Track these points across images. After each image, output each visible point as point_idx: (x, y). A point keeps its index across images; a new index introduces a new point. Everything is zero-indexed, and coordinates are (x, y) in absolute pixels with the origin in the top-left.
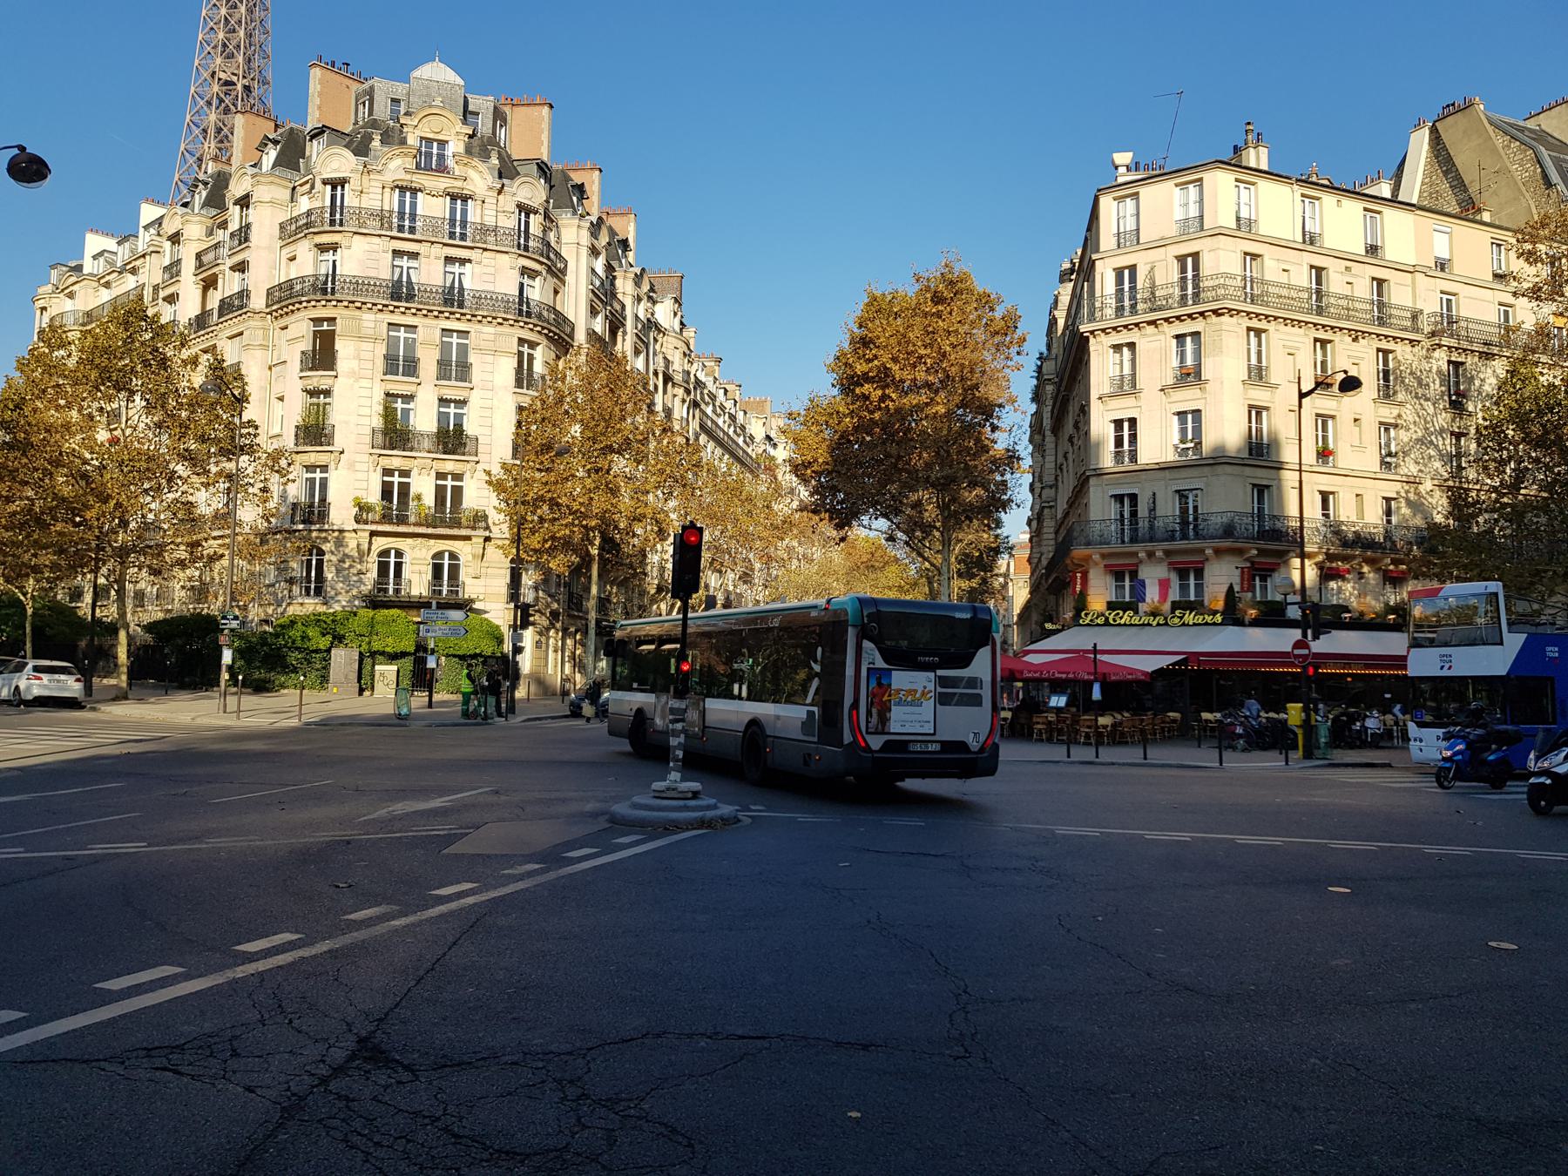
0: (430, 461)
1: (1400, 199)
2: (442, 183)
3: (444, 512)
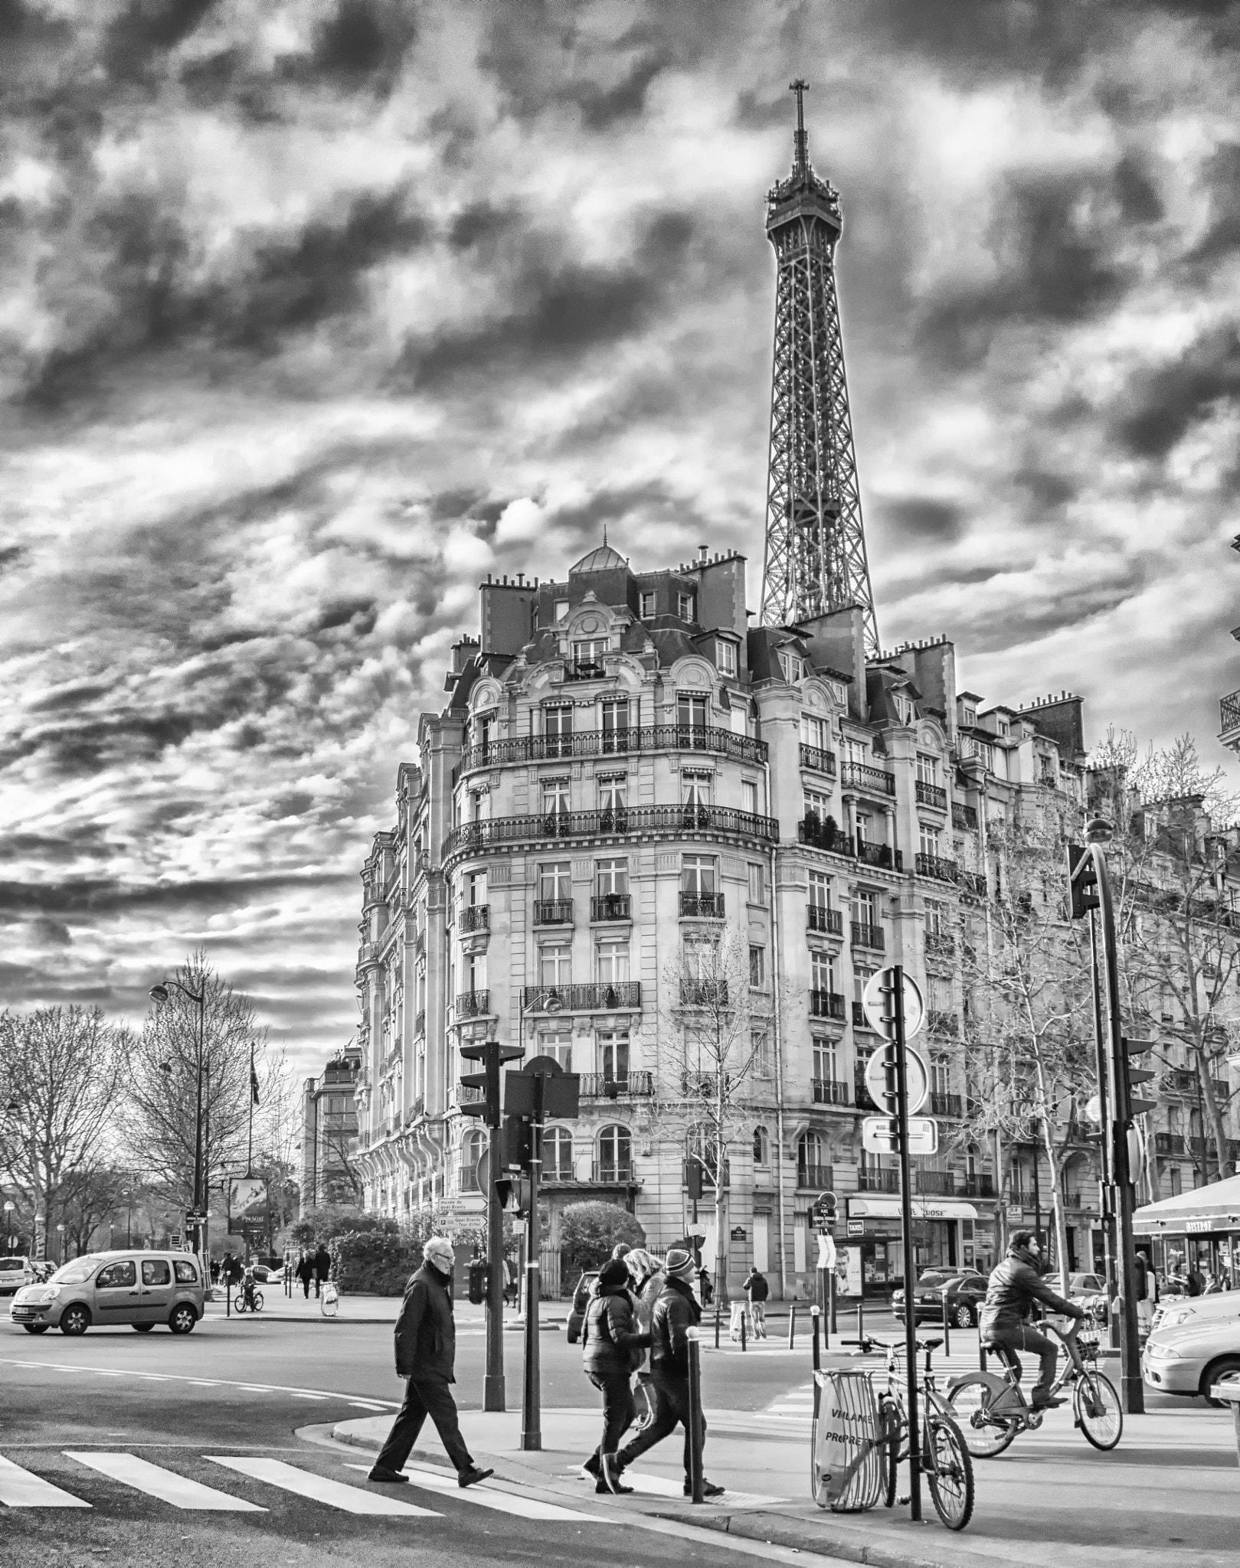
0: (588, 1020)
2: (594, 689)
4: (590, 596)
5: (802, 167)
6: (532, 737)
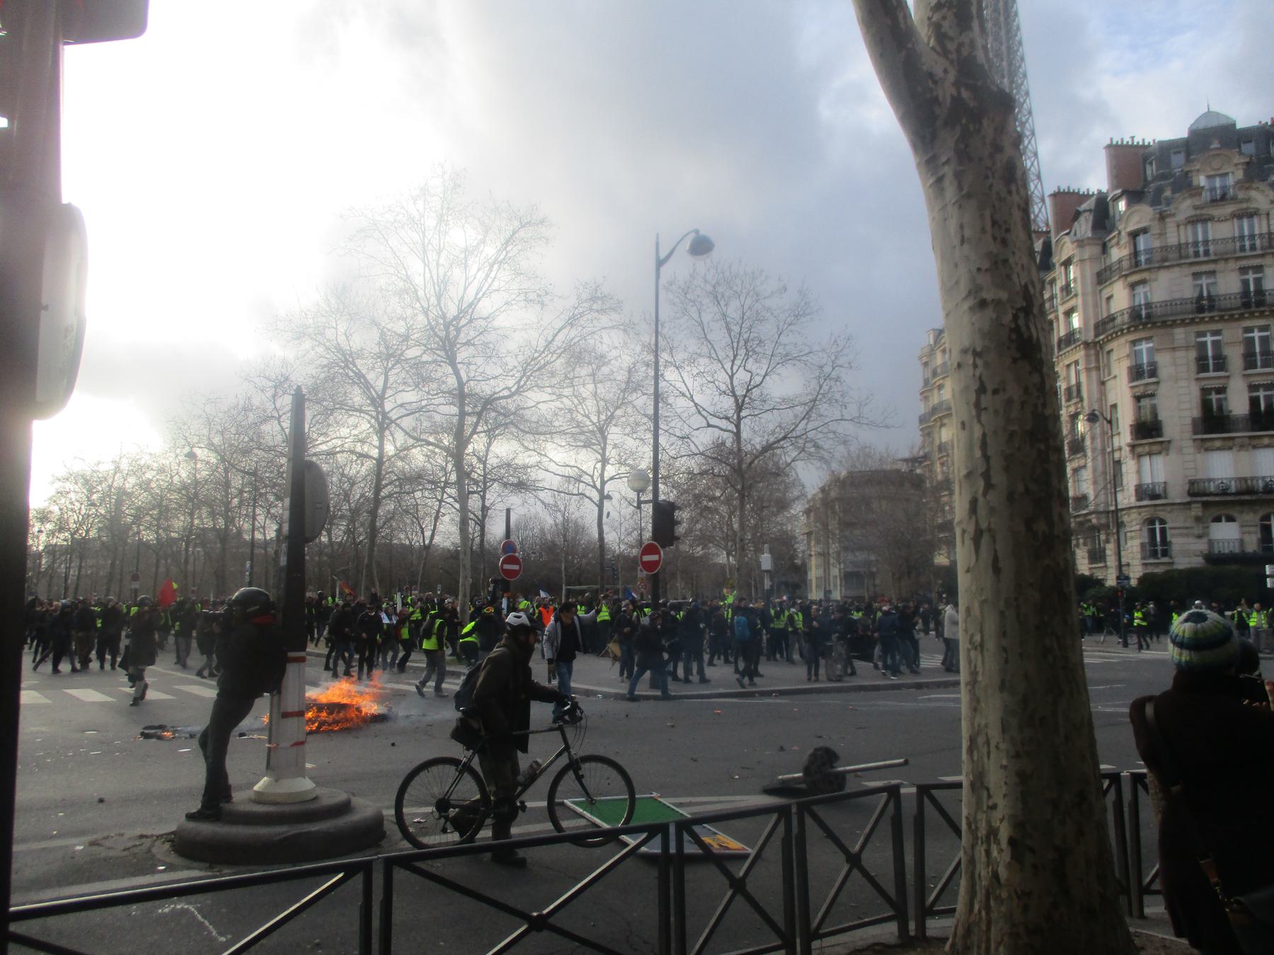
4: (1215, 145)
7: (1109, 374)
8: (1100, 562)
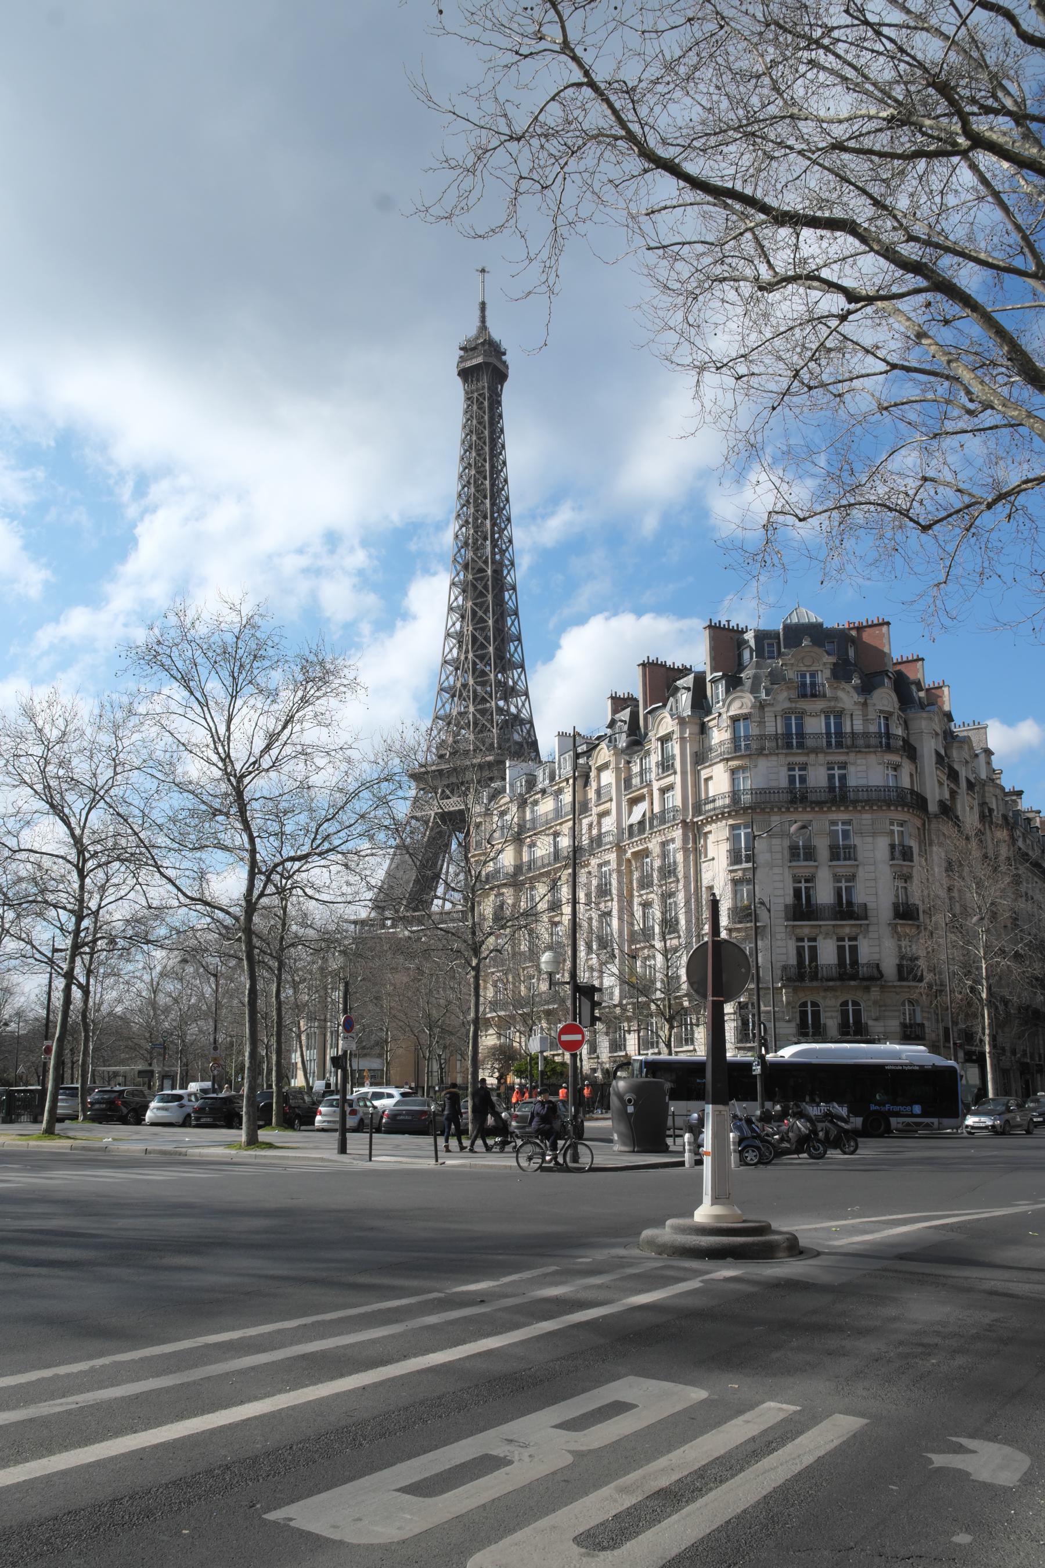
1: (348, 1135)
2: (820, 705)
3: (845, 967)
5: (483, 327)
6: (777, 734)
7: (706, 856)
8: (621, 1050)
